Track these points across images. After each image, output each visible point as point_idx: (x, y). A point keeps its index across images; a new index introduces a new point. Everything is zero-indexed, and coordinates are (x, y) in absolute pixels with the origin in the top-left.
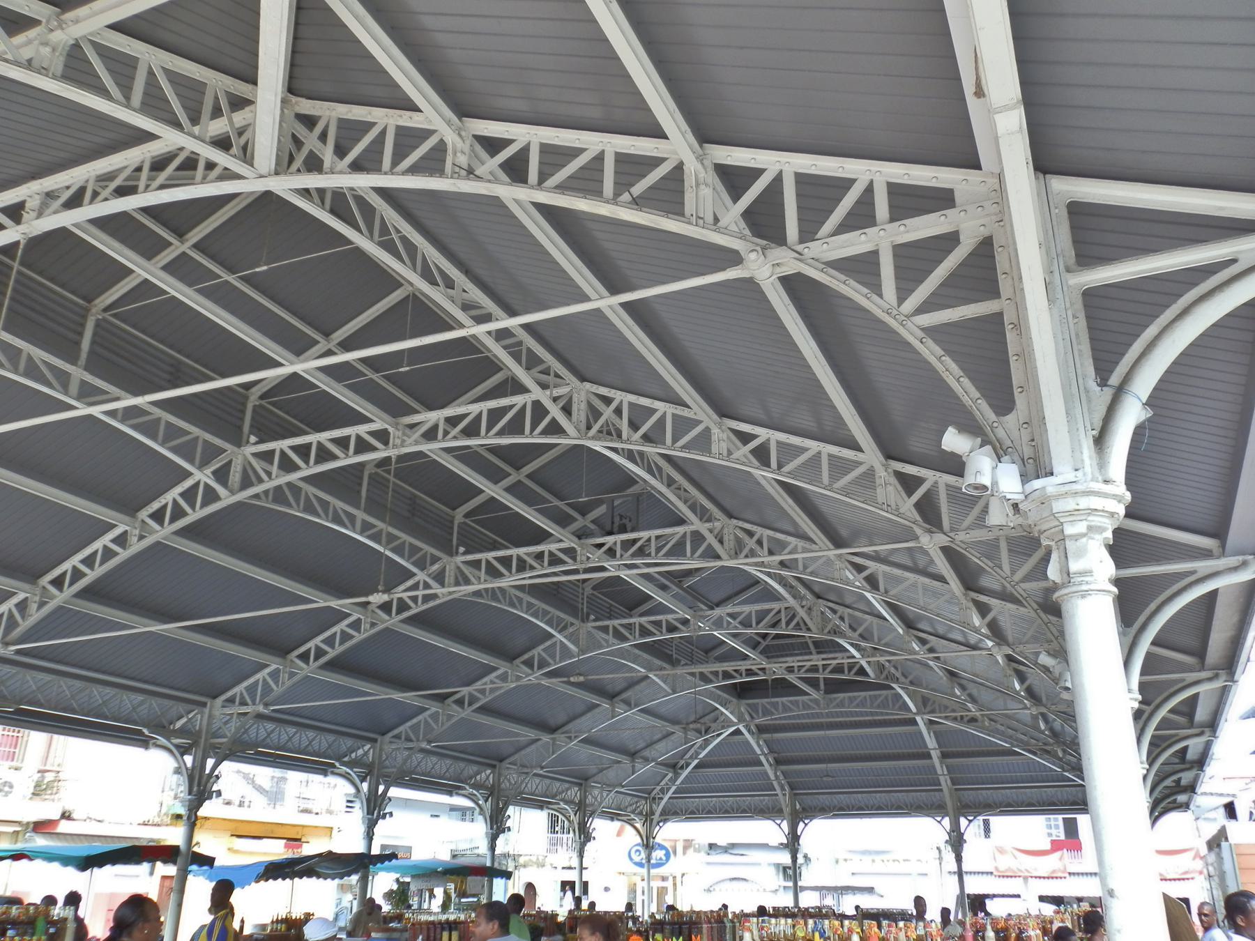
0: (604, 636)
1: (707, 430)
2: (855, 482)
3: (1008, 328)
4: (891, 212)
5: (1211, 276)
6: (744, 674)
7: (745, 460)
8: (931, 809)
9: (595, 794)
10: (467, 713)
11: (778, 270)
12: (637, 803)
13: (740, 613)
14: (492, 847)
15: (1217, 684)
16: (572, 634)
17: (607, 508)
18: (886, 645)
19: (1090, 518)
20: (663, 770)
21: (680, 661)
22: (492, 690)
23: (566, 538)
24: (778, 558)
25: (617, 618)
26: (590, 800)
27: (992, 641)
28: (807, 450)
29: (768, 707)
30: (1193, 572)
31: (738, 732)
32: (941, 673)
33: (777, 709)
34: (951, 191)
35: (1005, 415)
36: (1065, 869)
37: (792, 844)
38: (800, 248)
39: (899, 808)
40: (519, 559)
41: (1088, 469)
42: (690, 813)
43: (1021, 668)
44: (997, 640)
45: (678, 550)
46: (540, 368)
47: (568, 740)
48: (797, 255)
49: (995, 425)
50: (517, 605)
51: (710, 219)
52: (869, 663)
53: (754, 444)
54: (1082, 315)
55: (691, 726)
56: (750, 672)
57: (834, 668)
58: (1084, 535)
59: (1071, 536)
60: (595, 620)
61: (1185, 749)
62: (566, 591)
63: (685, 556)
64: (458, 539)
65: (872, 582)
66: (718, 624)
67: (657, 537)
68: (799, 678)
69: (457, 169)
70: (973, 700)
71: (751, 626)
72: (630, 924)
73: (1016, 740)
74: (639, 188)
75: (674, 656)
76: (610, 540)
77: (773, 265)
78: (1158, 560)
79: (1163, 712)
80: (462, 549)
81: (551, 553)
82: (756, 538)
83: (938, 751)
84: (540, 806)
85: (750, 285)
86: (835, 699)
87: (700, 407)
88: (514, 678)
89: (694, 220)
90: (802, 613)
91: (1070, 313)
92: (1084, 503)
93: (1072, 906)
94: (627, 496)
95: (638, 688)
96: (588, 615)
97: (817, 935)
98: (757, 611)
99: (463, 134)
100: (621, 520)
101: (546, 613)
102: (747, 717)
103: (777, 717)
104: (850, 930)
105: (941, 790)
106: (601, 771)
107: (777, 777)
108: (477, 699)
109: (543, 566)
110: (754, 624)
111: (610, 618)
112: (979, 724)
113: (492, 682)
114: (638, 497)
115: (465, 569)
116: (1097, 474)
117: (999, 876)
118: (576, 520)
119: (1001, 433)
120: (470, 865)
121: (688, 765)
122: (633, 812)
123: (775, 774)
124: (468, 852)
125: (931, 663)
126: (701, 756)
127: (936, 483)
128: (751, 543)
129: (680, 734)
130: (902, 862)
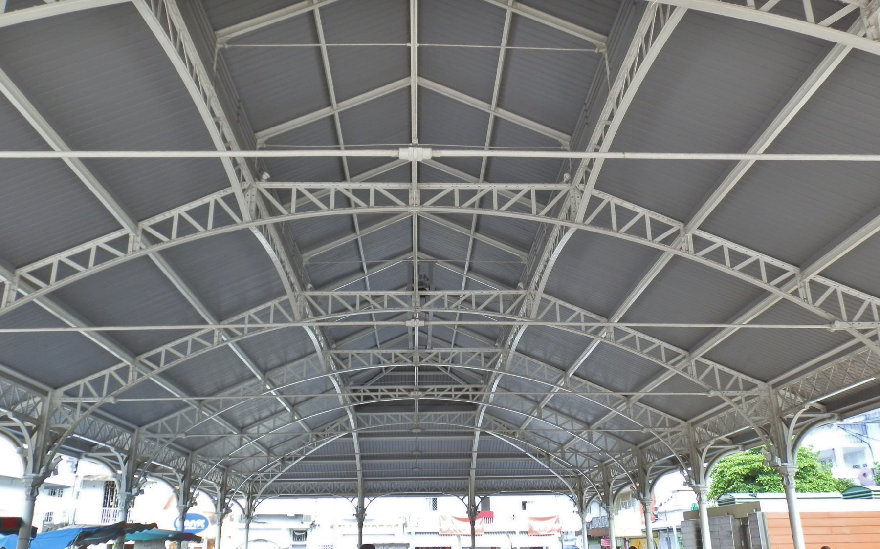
5: (265, 237)
8: (347, 492)
36: (483, 529)
42: (283, 493)
63: (444, 307)
86: (426, 415)
105: (357, 480)
117: (441, 535)
130: (378, 526)
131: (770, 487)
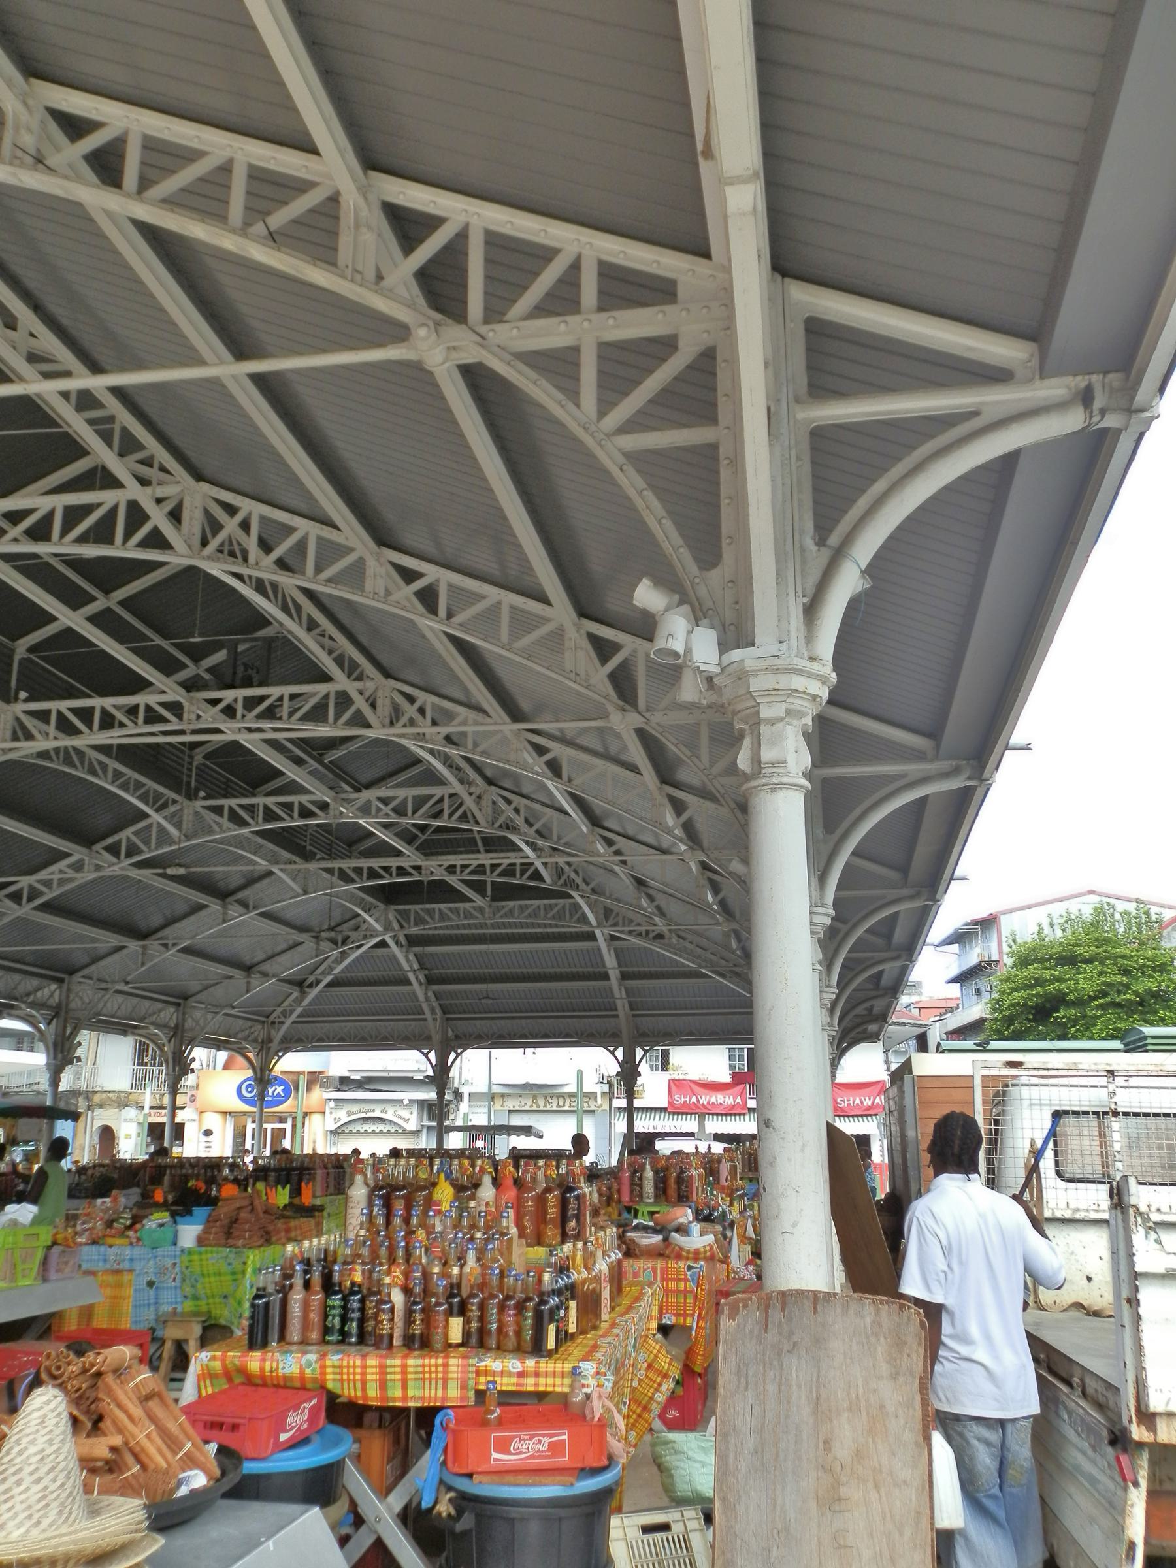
0: (217, 818)
1: (361, 561)
2: (479, 616)
3: (723, 462)
4: (600, 299)
6: (394, 874)
7: (407, 604)
9: (197, 1015)
10: (26, 910)
11: (454, 355)
12: (160, 1011)
13: (394, 798)
14: (55, 1082)
15: (917, 904)
16: (173, 815)
17: (229, 652)
18: (567, 844)
19: (790, 700)
20: (287, 988)
21: (315, 854)
22: (62, 882)
23: (170, 688)
24: (445, 730)
25: (235, 797)
26: (189, 1023)
27: (685, 844)
28: (484, 597)
29: (422, 914)
30: (902, 776)
31: (383, 944)
32: (628, 882)
33: (432, 918)
34: (673, 283)
35: (708, 570)
37: (441, 1077)
38: (483, 329)
39: (567, 1036)
40: (104, 712)
41: (794, 642)
42: (318, 1041)
43: (716, 877)
44: (690, 844)
45: (317, 714)
46: (140, 455)
47: (163, 949)
48: (478, 339)
49: (697, 580)
50: (100, 772)
51: (371, 275)
52: (545, 864)
53: (419, 584)
54: (807, 458)
55: (324, 935)
56: (401, 871)
57: (504, 870)
58: (781, 719)
59: (767, 720)
60: (204, 798)
61: (881, 973)
62: (168, 758)
64: (18, 680)
65: (554, 767)
66: (365, 810)
67: (293, 697)
68: (463, 881)
69: (19, 153)
70: (661, 912)
71: (406, 815)
72: (227, 1171)
73: (705, 961)
74: (278, 219)
75: (309, 848)
76: (228, 695)
77: (448, 348)
78: (879, 759)
79: (859, 932)
80: (23, 695)
81: (148, 708)
82: (417, 705)
83: (617, 972)
84: (124, 1030)
85: (417, 372)
86: (503, 907)
87: (353, 529)
88: (92, 868)
89: (349, 272)
90: (469, 803)
91: (793, 453)
92: (785, 681)
93: (744, 1145)
94: (256, 639)
95: (258, 885)
96: (197, 790)
97: (442, 1176)
98: (414, 797)
99: (31, 102)
100: (246, 670)
101: (139, 785)
102: (396, 926)
103: (432, 927)
104: (482, 1170)
105: (617, 1016)
106: (206, 988)
107: (427, 999)
108: (40, 894)
109: (136, 724)
110: (410, 812)
111: (225, 797)
112: (666, 941)
113: (61, 871)
114: (270, 642)
115: (26, 720)
116: (804, 650)
118: (185, 666)
119: (702, 591)
120: (28, 1105)
121: (318, 982)
122: (245, 1039)
123: (426, 994)
124: (25, 1089)
125: (617, 869)
126: (336, 971)
127: (635, 651)
128: (411, 711)
129: (309, 945)
131: (1078, 1030)
